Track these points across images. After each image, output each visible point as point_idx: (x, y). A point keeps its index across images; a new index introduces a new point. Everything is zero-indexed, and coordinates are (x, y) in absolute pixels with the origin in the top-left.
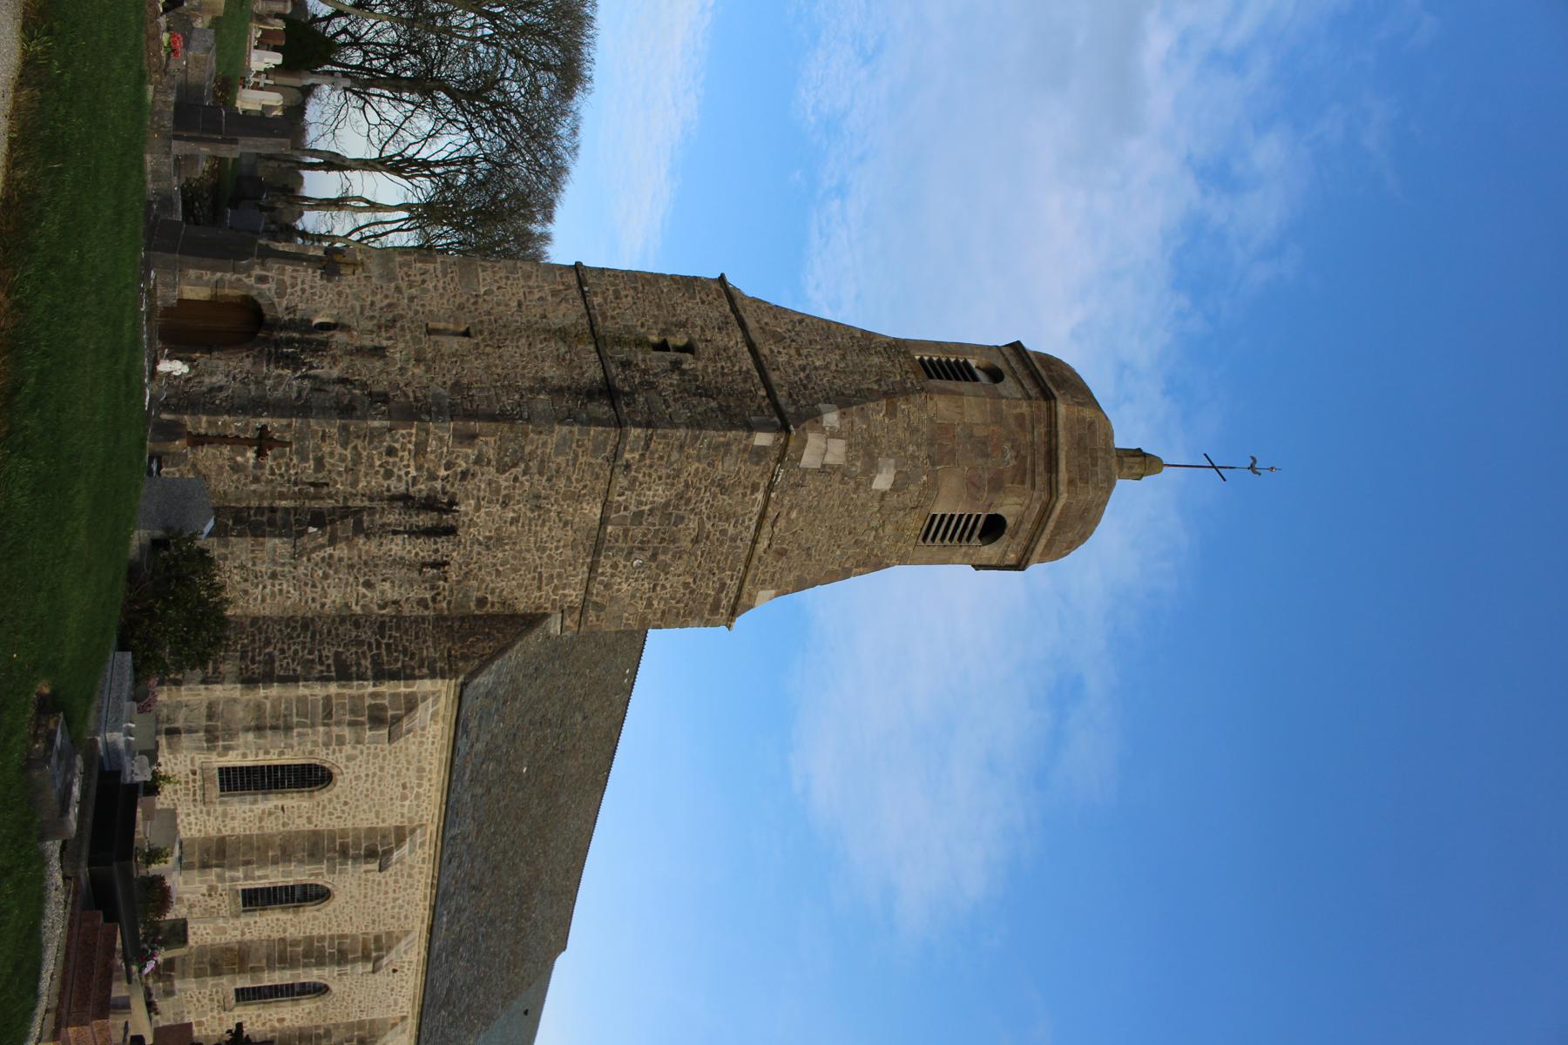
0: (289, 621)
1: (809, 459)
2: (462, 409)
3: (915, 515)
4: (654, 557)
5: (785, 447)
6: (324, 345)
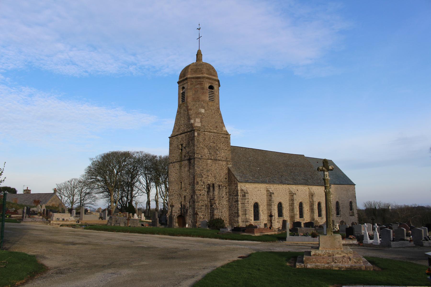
0: (229, 210)
1: (199, 125)
2: (193, 184)
3: (209, 103)
4: (217, 150)
5: (197, 130)
6: (184, 205)
